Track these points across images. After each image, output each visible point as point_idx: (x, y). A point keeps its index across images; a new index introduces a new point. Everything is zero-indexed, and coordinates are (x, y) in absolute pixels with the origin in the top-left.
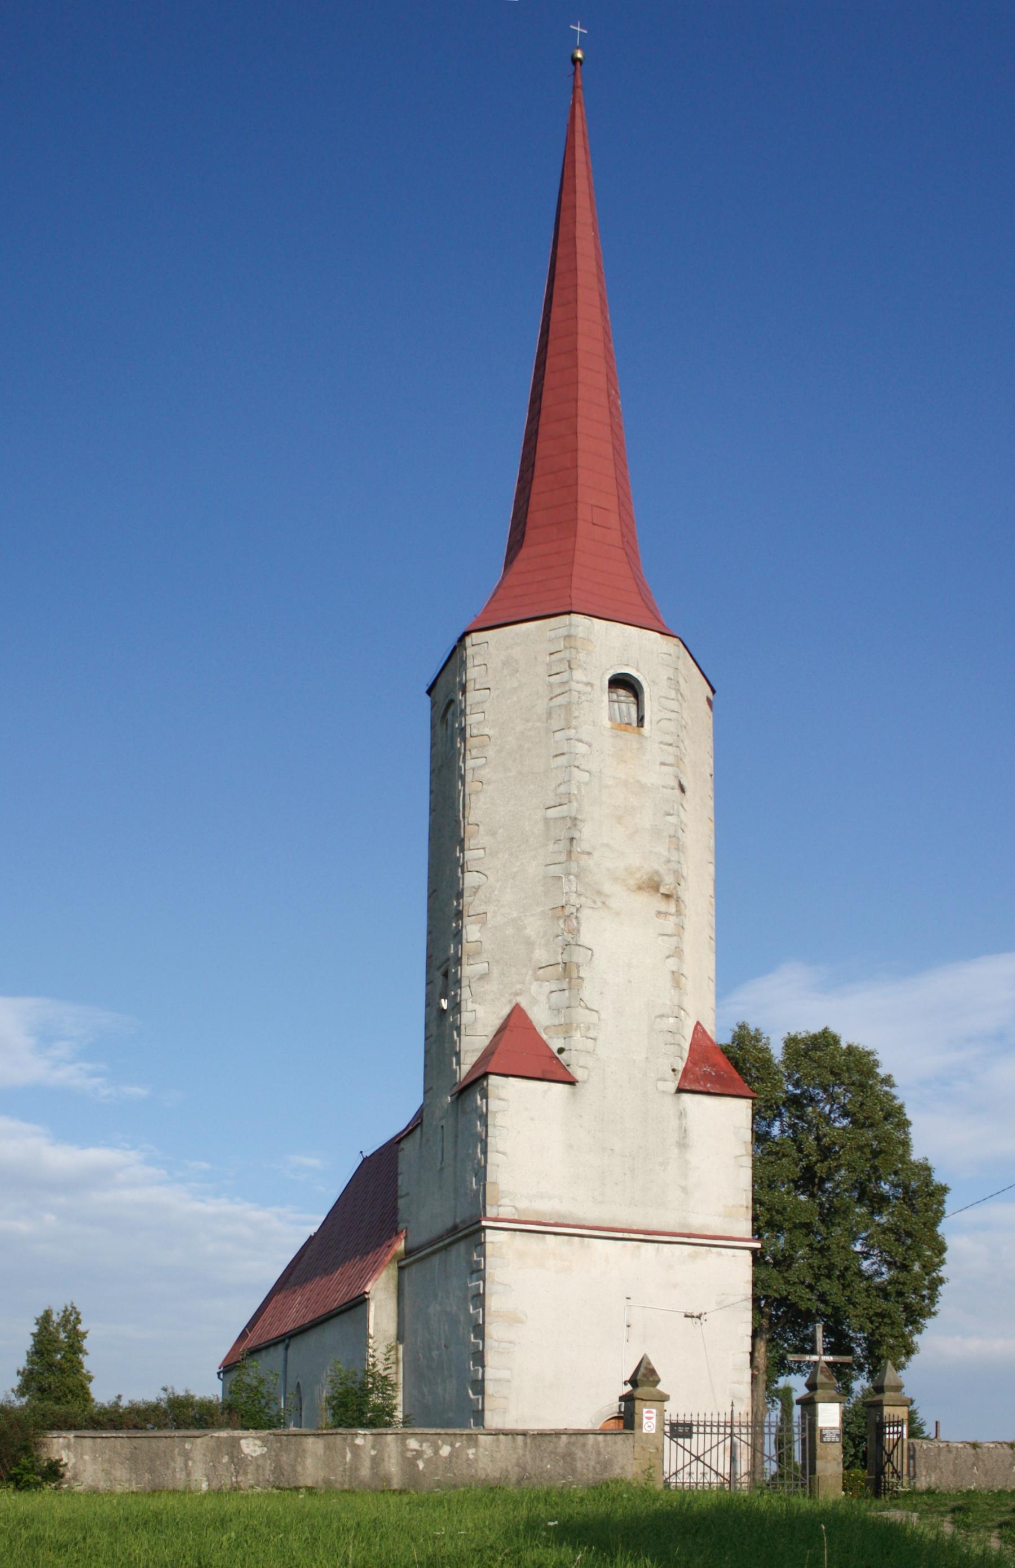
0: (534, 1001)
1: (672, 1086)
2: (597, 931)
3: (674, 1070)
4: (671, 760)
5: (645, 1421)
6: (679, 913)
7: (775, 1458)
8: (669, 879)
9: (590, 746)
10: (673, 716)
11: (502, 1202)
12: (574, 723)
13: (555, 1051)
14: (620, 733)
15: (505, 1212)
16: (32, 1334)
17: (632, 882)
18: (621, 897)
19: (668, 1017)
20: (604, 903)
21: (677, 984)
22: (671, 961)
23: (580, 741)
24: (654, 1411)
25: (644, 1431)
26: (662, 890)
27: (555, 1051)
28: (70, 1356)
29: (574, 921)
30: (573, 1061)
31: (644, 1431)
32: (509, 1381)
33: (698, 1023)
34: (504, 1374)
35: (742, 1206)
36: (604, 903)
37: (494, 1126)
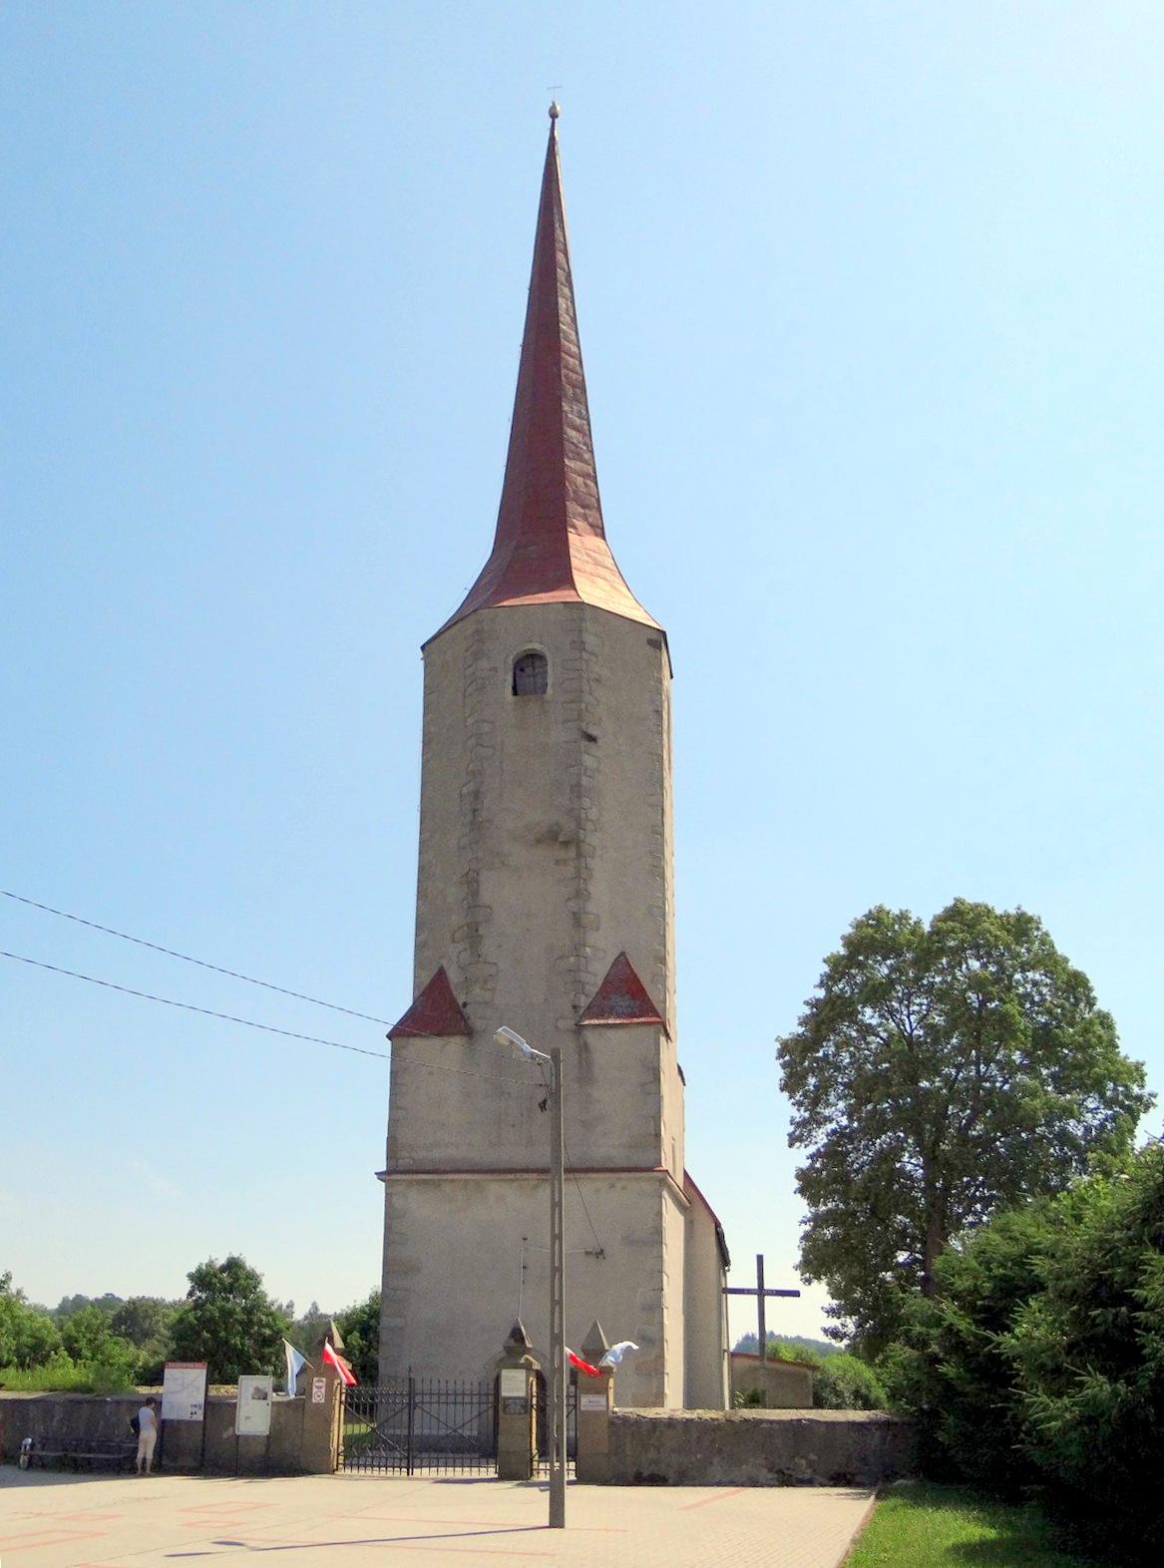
2: (497, 890)
3: (574, 1007)
5: (315, 1390)
9: (492, 723)
13: (460, 1004)
22: (571, 903)
23: (484, 721)
24: (324, 1379)
27: (460, 1004)
28: (822, 1185)
31: (314, 1401)
32: (402, 1329)
33: (623, 954)
34: (399, 1321)
35: (650, 1135)
36: (503, 863)
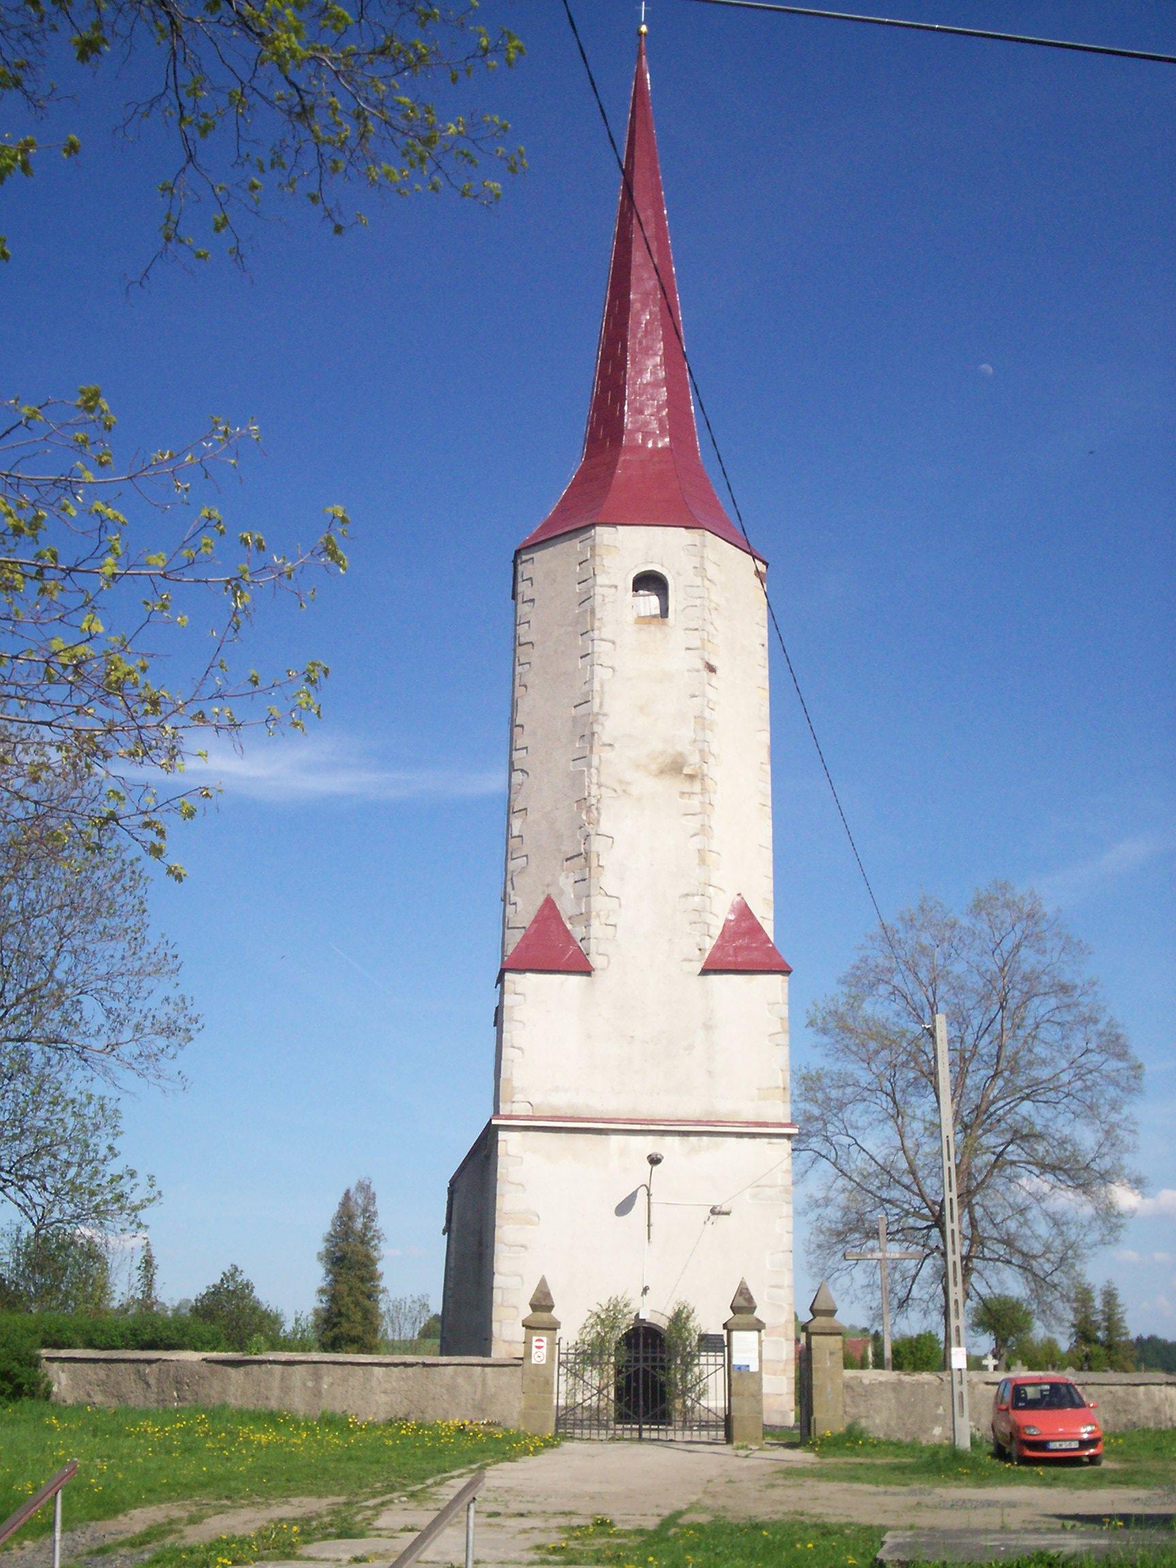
0: (562, 892)
1: (699, 967)
4: (698, 643)
6: (704, 790)
7: (1079, 1389)
8: (695, 759)
10: (698, 602)
11: (517, 1097)
12: (597, 624)
14: (643, 626)
15: (520, 1108)
16: (787, 1171)
17: (654, 767)
18: (647, 785)
19: (693, 895)
20: (624, 791)
21: (703, 861)
24: (545, 1339)
25: (534, 1362)
26: (686, 771)
29: (595, 812)
30: (593, 949)
31: (534, 1362)
37: (512, 1020)
